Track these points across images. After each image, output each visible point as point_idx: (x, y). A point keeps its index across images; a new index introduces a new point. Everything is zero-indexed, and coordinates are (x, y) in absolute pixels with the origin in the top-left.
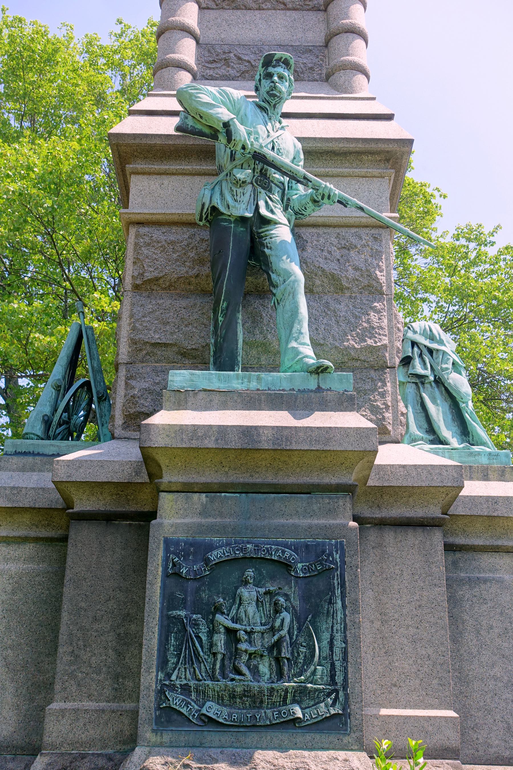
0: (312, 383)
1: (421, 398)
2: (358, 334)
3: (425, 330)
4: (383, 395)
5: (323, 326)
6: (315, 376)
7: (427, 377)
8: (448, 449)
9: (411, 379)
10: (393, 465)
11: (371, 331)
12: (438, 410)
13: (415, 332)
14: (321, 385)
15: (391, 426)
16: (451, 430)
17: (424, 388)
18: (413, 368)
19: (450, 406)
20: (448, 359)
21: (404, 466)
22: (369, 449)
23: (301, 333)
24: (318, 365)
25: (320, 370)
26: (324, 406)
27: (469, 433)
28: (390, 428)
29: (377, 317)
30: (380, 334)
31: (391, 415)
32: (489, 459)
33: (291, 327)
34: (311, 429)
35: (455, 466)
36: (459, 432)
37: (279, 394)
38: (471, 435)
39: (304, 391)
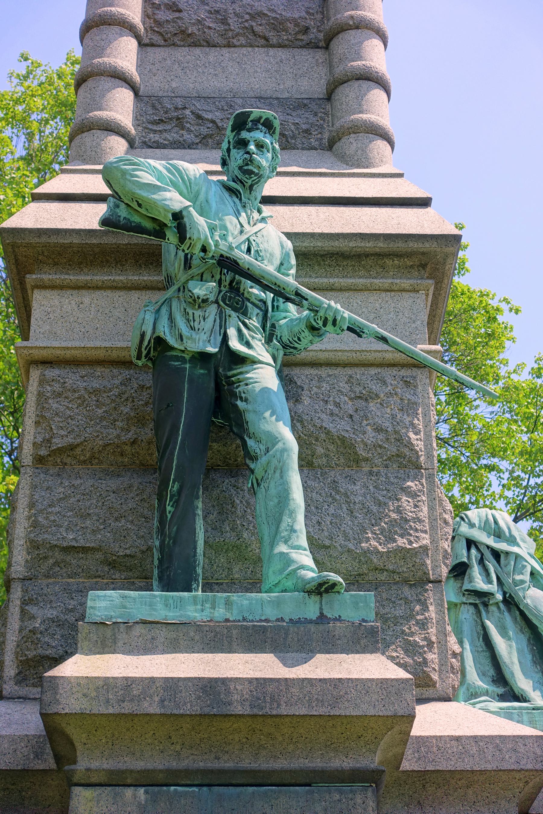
0: (311, 609)
1: (484, 627)
2: (382, 530)
4: (423, 625)
5: (329, 519)
6: (315, 598)
8: (527, 708)
9: (467, 598)
10: (441, 737)
11: (403, 525)
12: (510, 646)
13: (472, 525)
15: (437, 674)
16: (531, 678)
17: (487, 612)
18: (471, 582)
19: (529, 640)
20: (524, 567)
21: (458, 739)
25: (323, 589)
26: (331, 646)
28: (435, 677)
29: (411, 504)
30: (416, 530)
31: (436, 656)
35: (537, 736)
37: (260, 626)
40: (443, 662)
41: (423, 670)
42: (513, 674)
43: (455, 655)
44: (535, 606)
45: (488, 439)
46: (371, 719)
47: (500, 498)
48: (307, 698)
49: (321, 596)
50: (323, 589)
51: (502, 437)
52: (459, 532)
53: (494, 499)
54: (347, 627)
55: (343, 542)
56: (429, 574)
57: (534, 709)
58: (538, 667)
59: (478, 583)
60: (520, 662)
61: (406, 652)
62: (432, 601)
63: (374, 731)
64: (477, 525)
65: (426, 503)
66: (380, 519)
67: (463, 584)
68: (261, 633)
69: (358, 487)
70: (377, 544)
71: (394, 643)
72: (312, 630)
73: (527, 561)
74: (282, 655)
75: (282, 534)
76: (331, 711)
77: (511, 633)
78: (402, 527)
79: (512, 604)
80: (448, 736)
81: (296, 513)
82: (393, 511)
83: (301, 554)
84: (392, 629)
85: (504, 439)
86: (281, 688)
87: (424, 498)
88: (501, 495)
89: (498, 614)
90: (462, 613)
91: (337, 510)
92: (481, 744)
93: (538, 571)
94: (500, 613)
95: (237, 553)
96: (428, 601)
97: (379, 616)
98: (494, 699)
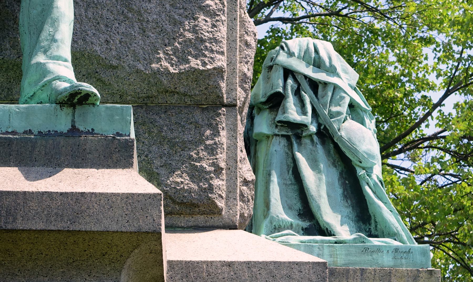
0: (63, 123)
1: (295, 161)
2: (175, 51)
3: (307, 51)
4: (212, 150)
5: (119, 37)
6: (67, 110)
7: (305, 126)
8: (329, 242)
9: (280, 130)
10: (212, 262)
11: (198, 46)
12: (320, 179)
13: (290, 54)
14: (77, 125)
15: (223, 201)
16: (340, 212)
17: (300, 144)
18: (284, 113)
19: (341, 174)
20: (342, 98)
21: (230, 264)
22: (145, 228)
23: (54, 40)
24: (71, 91)
25: (75, 100)
26: (80, 160)
27: (370, 217)
28: (221, 204)
29: (209, 24)
30: (212, 51)
31: (224, 183)
32: (395, 258)
33: (40, 30)
34: (50, 195)
35: (314, 263)
36: (353, 215)
37: (5, 138)
38: (373, 221)
39: (49, 134)
40: (231, 189)
41: (208, 196)
42: (319, 207)
43: (246, 182)
44: (349, 139)
45: (425, 10)
46: (115, 235)
47: (433, 70)
48: (46, 213)
49: (74, 108)
50: (76, 100)
51: (439, 9)
52: (277, 61)
53: (427, 72)
54: (99, 141)
55: (131, 62)
56: (222, 97)
57: (336, 243)
58: (349, 201)
59: (292, 114)
60: (329, 196)
61: (192, 178)
62: (224, 125)
63: (119, 248)
64: (296, 55)
65: (225, 23)
66: (174, 39)
67: (276, 115)
68: (6, 145)
69: (152, 5)
70: (169, 65)
71: (179, 169)
72: (62, 143)
73: (345, 93)
74: (26, 168)
75: (42, 44)
76: (71, 226)
77: (322, 166)
78: (197, 48)
79: (327, 137)
80: (220, 261)
81: (59, 22)
82: (188, 30)
83: (59, 65)
84: (178, 154)
85: (441, 11)
86: (18, 201)
87: (223, 18)
88: (434, 68)
89: (311, 147)
90: (273, 145)
91: (128, 29)
92: (254, 270)
93: (358, 103)
94: (313, 146)
95: (18, 72)
96: (219, 126)
97: (167, 140)
98: (298, 233)
